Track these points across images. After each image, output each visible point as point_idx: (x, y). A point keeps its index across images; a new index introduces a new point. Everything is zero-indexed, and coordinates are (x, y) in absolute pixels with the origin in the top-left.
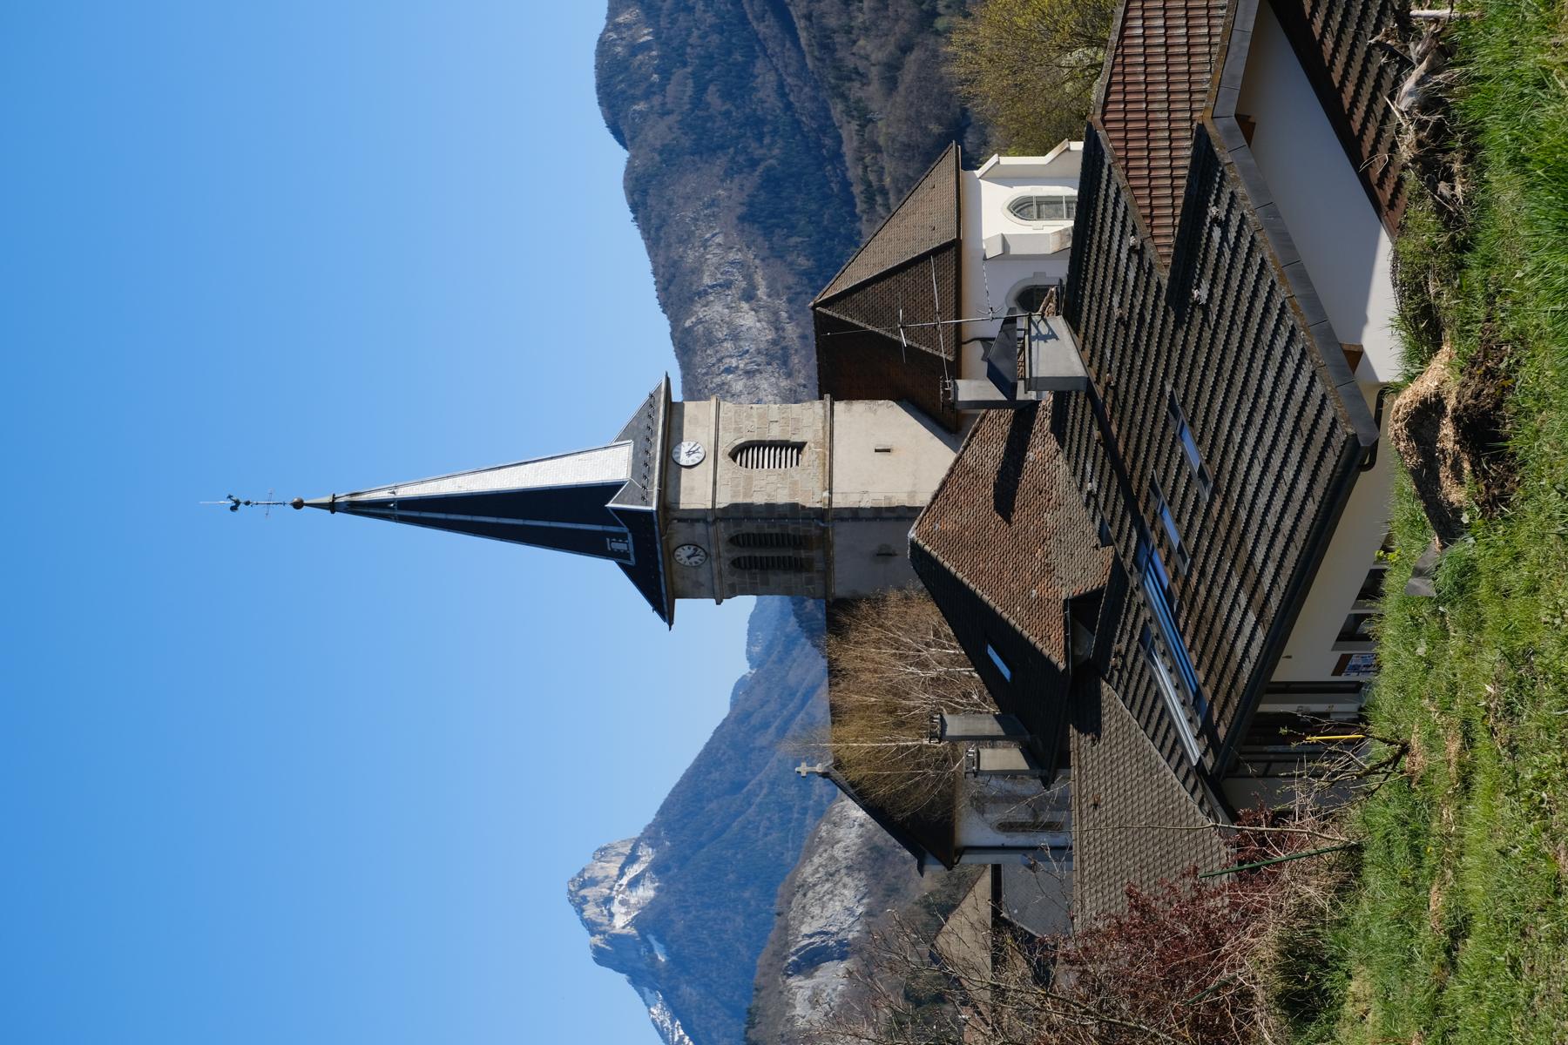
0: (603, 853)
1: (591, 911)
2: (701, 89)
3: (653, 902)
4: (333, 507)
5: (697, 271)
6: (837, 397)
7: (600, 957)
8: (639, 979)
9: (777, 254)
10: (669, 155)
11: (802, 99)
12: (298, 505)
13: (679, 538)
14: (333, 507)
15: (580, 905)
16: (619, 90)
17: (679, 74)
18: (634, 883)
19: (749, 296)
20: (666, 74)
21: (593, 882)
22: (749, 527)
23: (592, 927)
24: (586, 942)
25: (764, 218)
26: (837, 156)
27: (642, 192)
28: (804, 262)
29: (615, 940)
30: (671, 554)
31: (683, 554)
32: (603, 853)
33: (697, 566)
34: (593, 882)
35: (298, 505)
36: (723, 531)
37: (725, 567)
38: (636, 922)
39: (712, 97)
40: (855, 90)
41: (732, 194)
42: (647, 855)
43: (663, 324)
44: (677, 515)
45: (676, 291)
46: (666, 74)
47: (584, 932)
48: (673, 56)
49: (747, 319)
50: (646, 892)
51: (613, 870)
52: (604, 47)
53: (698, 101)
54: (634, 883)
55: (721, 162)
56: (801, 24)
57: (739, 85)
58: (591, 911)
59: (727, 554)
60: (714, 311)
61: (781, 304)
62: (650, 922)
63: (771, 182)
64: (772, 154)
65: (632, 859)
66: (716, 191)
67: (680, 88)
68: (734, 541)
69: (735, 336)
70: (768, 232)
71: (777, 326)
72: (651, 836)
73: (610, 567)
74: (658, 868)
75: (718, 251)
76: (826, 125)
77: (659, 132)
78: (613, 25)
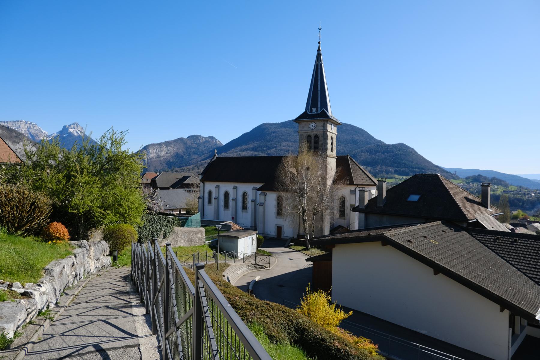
0: (82, 128)
1: (72, 126)
2: (194, 148)
3: (74, 135)
4: (319, 50)
5: (170, 146)
6: (337, 159)
7: (65, 127)
8: (61, 132)
9: (172, 157)
10: (186, 144)
11: (193, 161)
12: (319, 43)
13: (318, 123)
14: (319, 50)
15: (74, 124)
16: (194, 138)
17: (196, 146)
18: (77, 132)
19: (167, 153)
20: (196, 144)
21: (77, 126)
22: (321, 139)
23: (70, 126)
24: (67, 125)
25: (177, 156)
26: (186, 166)
27: (181, 140)
28: (171, 161)
29: (68, 129)
30: (313, 122)
31: (314, 124)
32: (82, 128)
33: (309, 127)
34: (77, 126)
35: (319, 43)
36: (320, 133)
37: (309, 134)
38: (70, 132)
39: (193, 150)
40: (196, 168)
41: (180, 152)
42: (82, 134)
43: (163, 141)
44: (326, 123)
45: (167, 143)
46: (196, 144)
47: (69, 124)
48: (199, 145)
49: (163, 153)
50: (76, 134)
51: (79, 129)
52: (200, 136)
53: (193, 148)
54: (77, 132)
55: (185, 150)
56: (204, 161)
57: (195, 153)
58: (72, 126)
59: (312, 134)
60: (165, 148)
61: (166, 157)
62: (71, 134)
63: (182, 157)
64: (186, 157)
65: (81, 132)
66: (181, 150)
67: (195, 146)
68: (316, 136)
69: (161, 151)
70: (175, 156)
71: (162, 157)
72: (85, 135)
73: (304, 111)
74: (79, 136)
75: (173, 150)
76: (190, 165)
77: (189, 142)
78: (203, 137)
